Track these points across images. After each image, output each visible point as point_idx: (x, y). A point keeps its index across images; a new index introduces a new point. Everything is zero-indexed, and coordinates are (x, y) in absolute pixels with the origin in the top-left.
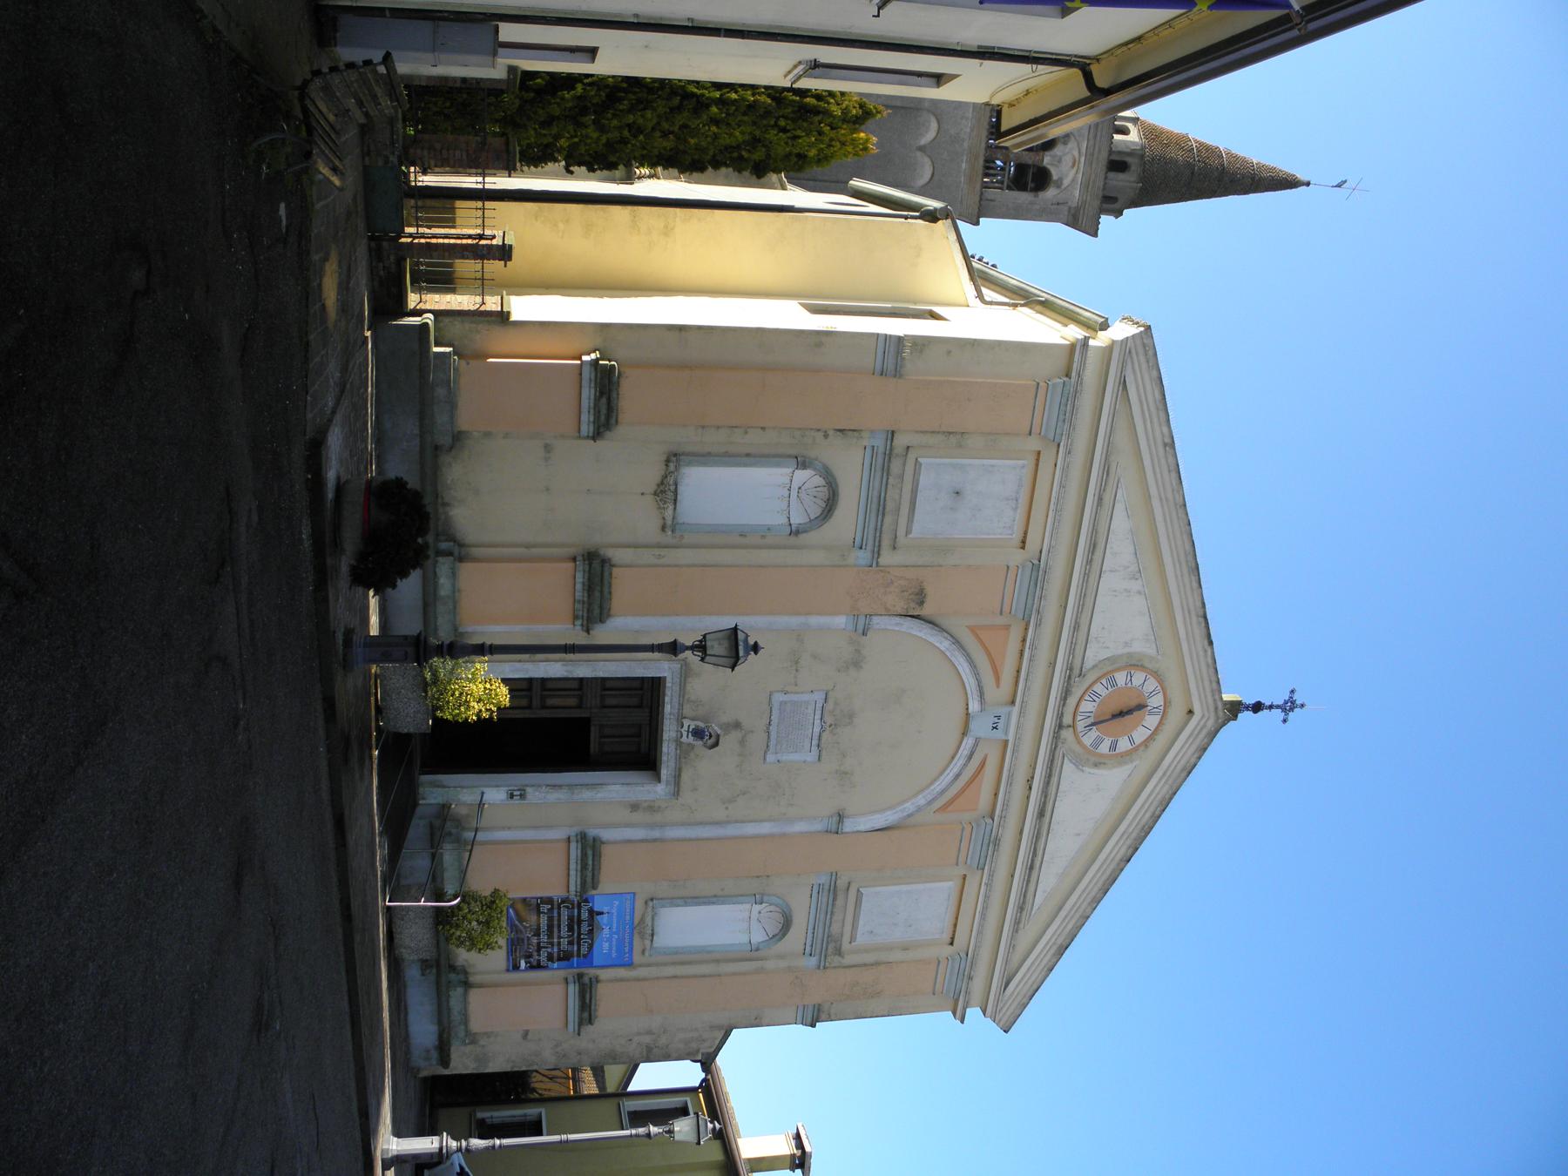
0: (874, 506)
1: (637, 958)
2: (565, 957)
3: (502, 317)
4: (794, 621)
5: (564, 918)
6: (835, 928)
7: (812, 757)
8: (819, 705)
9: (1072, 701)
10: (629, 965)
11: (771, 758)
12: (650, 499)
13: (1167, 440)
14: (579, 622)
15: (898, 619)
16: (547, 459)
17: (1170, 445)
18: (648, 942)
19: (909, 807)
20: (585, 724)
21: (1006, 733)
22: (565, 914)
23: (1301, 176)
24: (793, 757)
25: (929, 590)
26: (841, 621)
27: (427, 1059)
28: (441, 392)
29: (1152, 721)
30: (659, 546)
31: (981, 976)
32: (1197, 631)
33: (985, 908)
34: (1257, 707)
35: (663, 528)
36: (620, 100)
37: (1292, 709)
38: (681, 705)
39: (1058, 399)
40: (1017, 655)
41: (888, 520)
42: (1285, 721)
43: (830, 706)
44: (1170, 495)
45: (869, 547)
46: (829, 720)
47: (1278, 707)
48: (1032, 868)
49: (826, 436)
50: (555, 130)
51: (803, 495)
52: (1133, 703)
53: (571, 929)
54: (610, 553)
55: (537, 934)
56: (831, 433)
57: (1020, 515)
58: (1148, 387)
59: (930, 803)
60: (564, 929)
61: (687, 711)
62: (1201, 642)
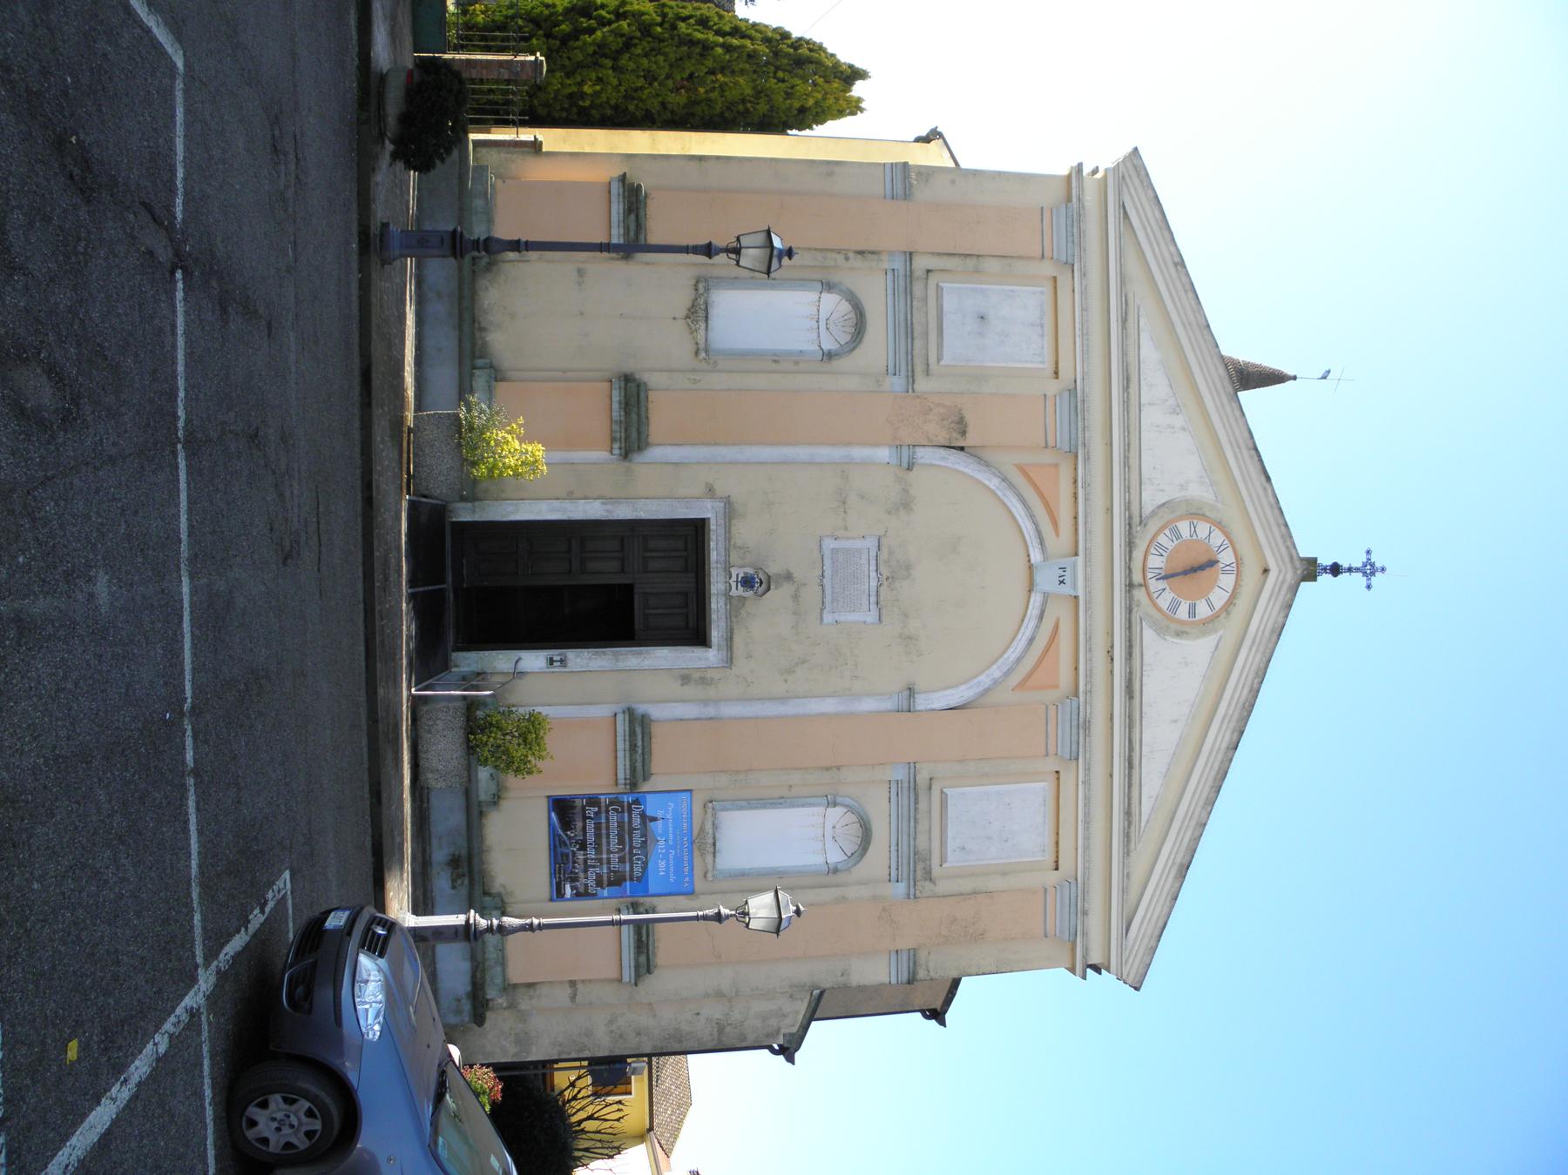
0: (903, 330)
1: (699, 885)
2: (617, 880)
3: (535, 146)
4: (837, 453)
5: (614, 825)
6: (922, 842)
7: (871, 617)
8: (873, 554)
9: (1138, 555)
10: (691, 893)
11: (828, 618)
12: (681, 324)
13: (1177, 259)
14: (616, 446)
15: (941, 451)
16: (580, 284)
17: (1180, 264)
18: (709, 858)
19: (984, 680)
20: (628, 589)
21: (1075, 586)
22: (614, 817)
23: (1291, 373)
24: (850, 617)
25: (969, 418)
26: (883, 454)
27: (459, 1012)
28: (478, 203)
29: (1227, 581)
30: (694, 370)
31: (1095, 926)
32: (1252, 469)
33: (1087, 814)
34: (1335, 570)
35: (697, 353)
36: (635, 46)
37: (1373, 574)
38: (727, 554)
39: (1063, 220)
40: (1072, 529)
41: (918, 343)
42: (1369, 587)
43: (884, 555)
44: (1192, 318)
45: (903, 373)
46: (885, 571)
47: (1357, 570)
48: (1131, 766)
49: (847, 259)
50: (579, 79)
51: (831, 327)
52: (1203, 559)
53: (621, 841)
54: (646, 377)
55: (583, 847)
56: (851, 255)
57: (1048, 341)
58: (1148, 210)
59: (1007, 674)
60: (614, 840)
61: (734, 558)
62: (1258, 479)
